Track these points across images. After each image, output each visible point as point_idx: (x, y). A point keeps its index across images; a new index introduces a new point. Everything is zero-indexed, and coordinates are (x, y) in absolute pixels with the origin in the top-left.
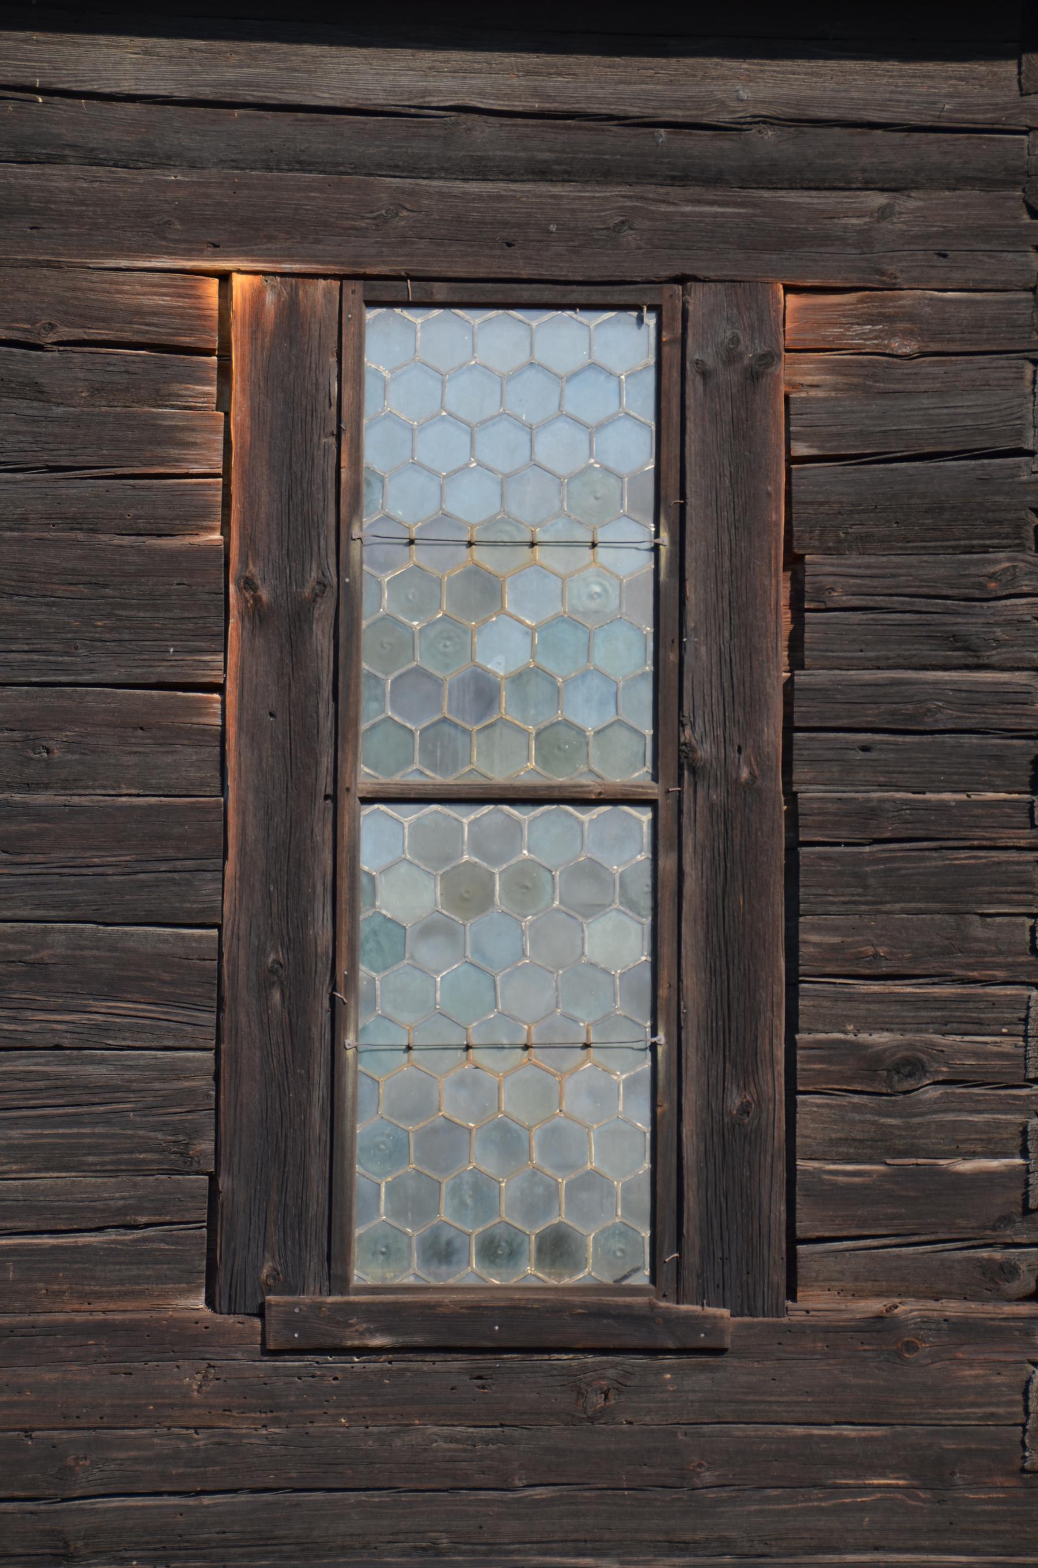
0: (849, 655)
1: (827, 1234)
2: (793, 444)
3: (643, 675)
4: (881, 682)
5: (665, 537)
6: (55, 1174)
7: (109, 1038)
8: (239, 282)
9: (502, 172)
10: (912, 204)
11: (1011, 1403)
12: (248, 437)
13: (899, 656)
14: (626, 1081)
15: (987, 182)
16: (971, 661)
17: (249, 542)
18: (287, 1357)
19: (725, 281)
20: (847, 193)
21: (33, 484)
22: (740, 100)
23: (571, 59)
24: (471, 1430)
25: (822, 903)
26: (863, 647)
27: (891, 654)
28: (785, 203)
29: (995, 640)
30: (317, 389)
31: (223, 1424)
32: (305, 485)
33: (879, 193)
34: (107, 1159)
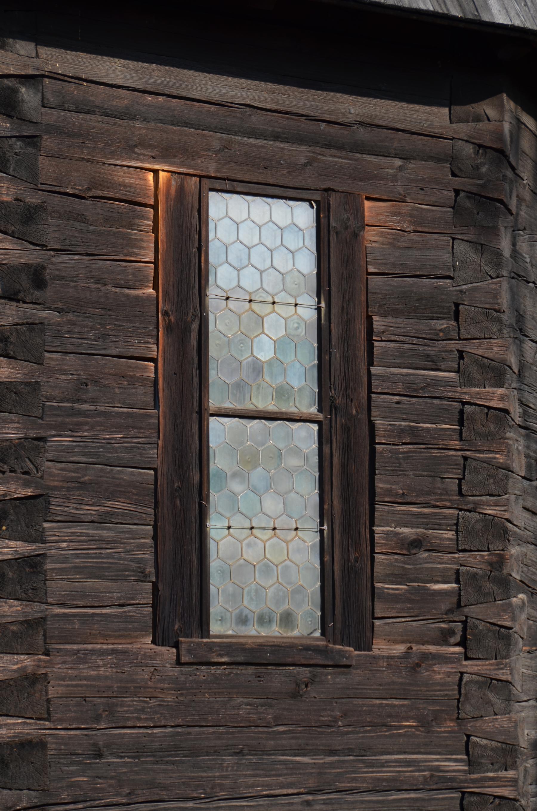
0: (390, 361)
1: (386, 616)
2: (368, 266)
3: (314, 365)
4: (403, 374)
5: (323, 305)
6: (93, 580)
7: (113, 518)
8: (162, 174)
9: (262, 135)
10: (412, 166)
11: (453, 690)
12: (165, 246)
13: (408, 363)
14: (311, 546)
15: (438, 159)
16: (434, 367)
17: (166, 293)
18: (186, 666)
19: (344, 192)
20: (388, 158)
21: (82, 261)
22: (350, 113)
23: (287, 88)
24: (255, 700)
25: (384, 470)
26: (395, 358)
27: (406, 362)
28: (366, 160)
29: (443, 358)
30: (191, 227)
31: (161, 696)
32: (187, 270)
33: (399, 159)
34: (113, 574)
